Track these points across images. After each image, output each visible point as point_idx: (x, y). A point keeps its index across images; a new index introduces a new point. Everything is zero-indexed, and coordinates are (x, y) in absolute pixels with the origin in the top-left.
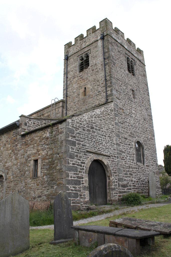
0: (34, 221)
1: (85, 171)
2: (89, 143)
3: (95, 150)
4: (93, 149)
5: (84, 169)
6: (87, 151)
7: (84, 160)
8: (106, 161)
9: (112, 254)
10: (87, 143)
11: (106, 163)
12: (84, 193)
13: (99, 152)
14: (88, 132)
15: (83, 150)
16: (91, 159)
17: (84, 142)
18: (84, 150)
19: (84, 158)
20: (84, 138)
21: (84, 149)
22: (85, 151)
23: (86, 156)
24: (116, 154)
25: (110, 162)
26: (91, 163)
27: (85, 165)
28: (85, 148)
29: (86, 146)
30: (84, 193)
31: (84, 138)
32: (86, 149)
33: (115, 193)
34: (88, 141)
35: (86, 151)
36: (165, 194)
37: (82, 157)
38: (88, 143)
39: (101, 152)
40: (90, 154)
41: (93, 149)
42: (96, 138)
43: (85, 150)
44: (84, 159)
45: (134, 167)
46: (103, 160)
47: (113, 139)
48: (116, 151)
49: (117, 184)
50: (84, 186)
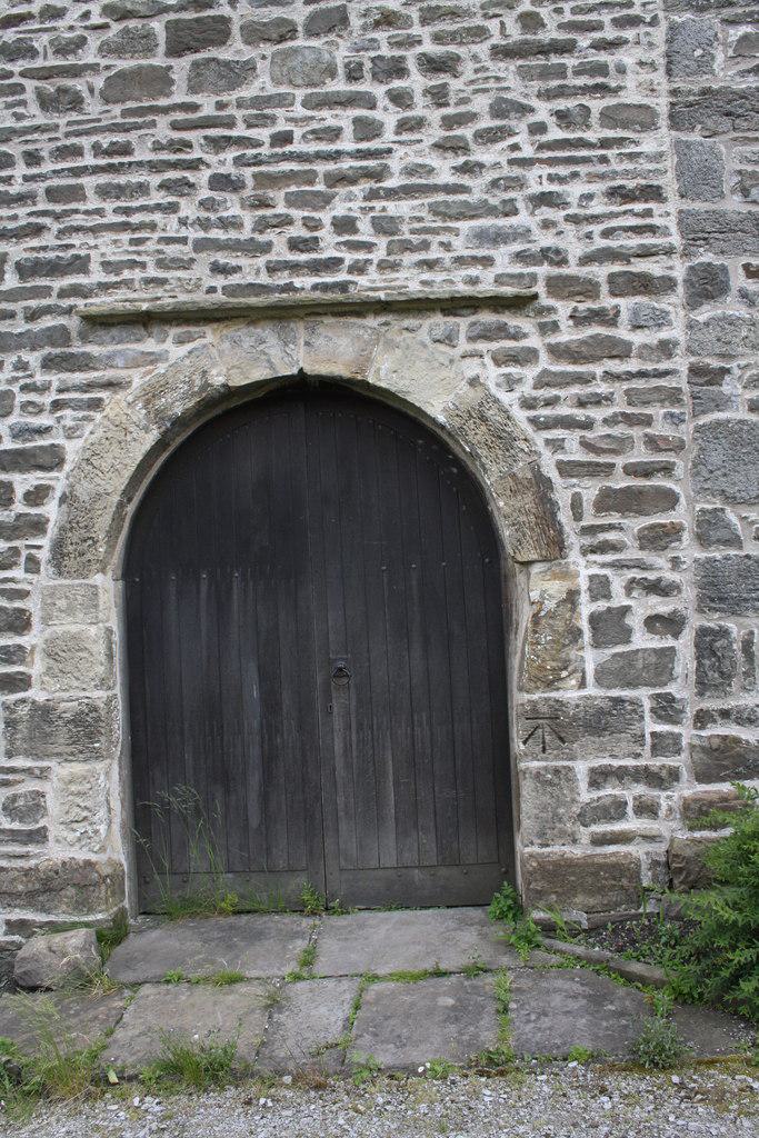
0: (581, 442)
1: (58, 548)
2: (136, 219)
3: (235, 279)
4: (201, 271)
5: (38, 526)
6: (99, 323)
7: (42, 431)
8: (430, 375)
9: (687, 817)
10: (94, 230)
11: (437, 404)
12: (32, 785)
13: (298, 282)
14: (117, 109)
15: (32, 316)
16: (150, 395)
17: (56, 227)
18: (48, 322)
19: (47, 399)
20: (52, 194)
21: (48, 310)
22: (64, 329)
23: (79, 377)
24: (669, 251)
25: (530, 373)
26: (151, 438)
27: (58, 481)
28: (76, 291)
29: (80, 264)
30: (32, 785)
31: (52, 194)
32: (80, 303)
33: (599, 777)
34: (109, 206)
35: (73, 323)
36: (332, 224)
37: (21, 398)
38: (125, 227)
39: (342, 276)
40: (150, 345)
41: (201, 271)
42: (263, 134)
43: (69, 311)
44: (44, 420)
45: (204, 341)
46: (384, 373)
47: (602, 69)
48: (674, 204)
49: (684, 645)
50: (23, 711)
